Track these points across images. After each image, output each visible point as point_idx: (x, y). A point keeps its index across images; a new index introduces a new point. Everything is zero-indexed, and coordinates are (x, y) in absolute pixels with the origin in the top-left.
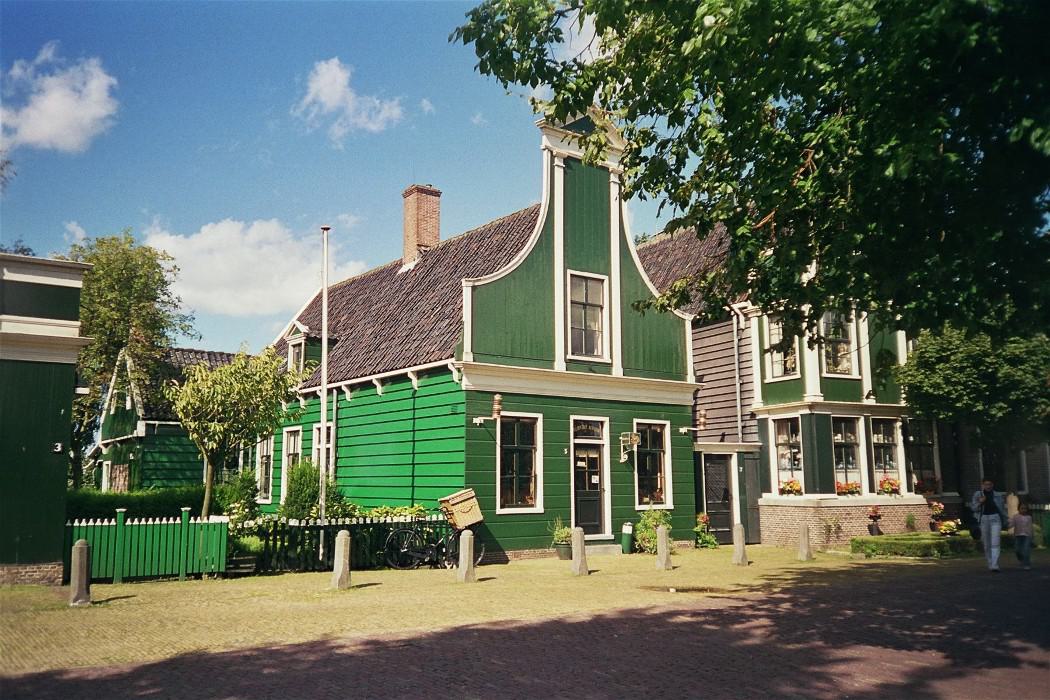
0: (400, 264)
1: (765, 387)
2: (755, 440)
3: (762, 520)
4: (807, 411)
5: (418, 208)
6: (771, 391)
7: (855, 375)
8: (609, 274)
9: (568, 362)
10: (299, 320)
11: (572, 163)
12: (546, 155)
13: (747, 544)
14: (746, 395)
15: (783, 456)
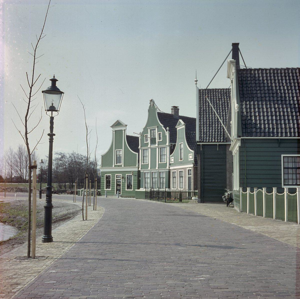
9: (115, 165)
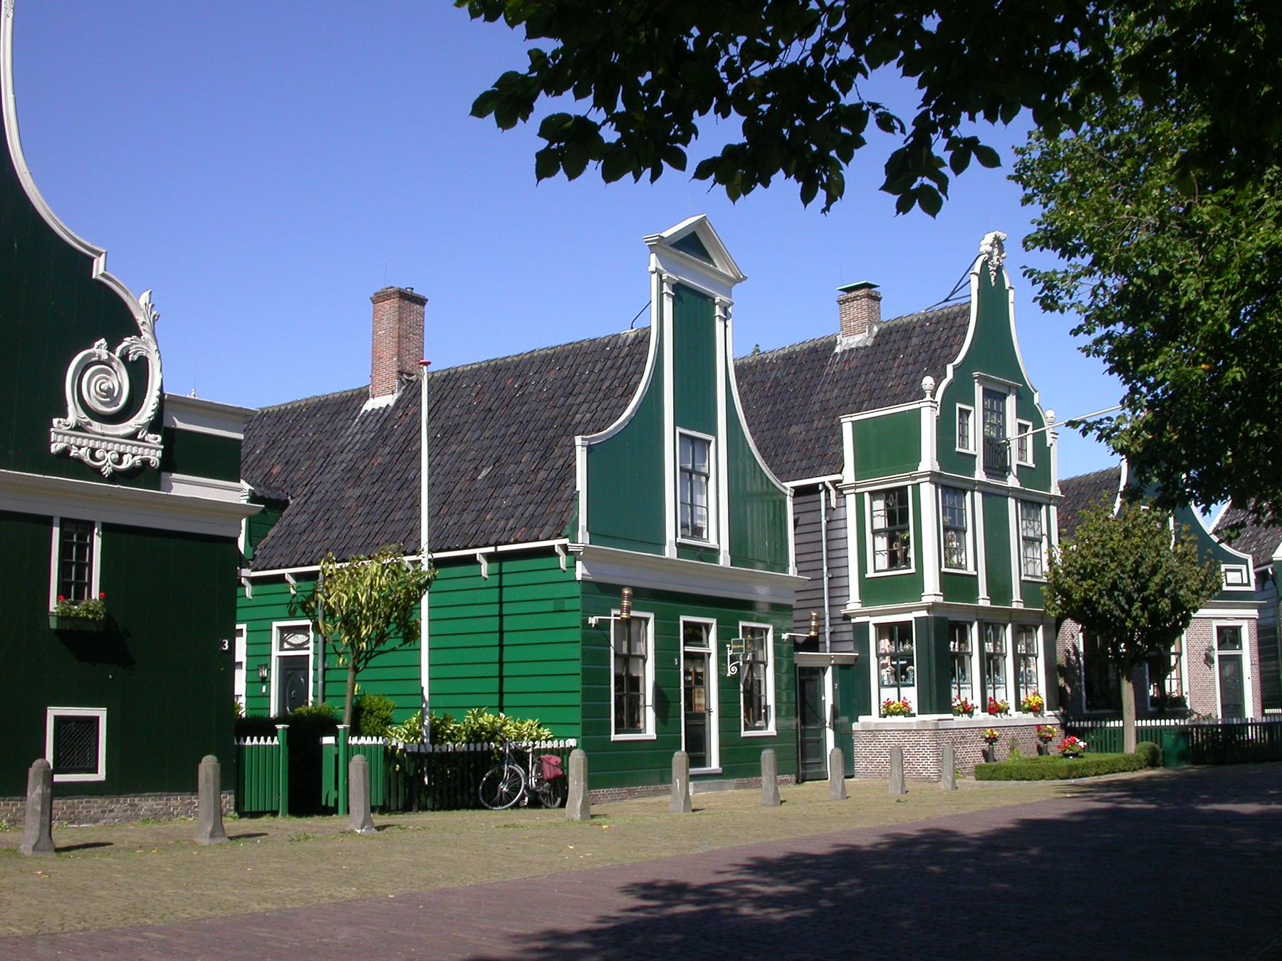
0: (363, 395)
1: (864, 583)
2: (849, 652)
3: (856, 750)
4: (924, 613)
5: (400, 320)
6: (873, 590)
7: (970, 570)
8: (714, 432)
9: (680, 546)
11: (685, 295)
12: (654, 277)
13: (846, 777)
14: (838, 593)
15: (884, 666)
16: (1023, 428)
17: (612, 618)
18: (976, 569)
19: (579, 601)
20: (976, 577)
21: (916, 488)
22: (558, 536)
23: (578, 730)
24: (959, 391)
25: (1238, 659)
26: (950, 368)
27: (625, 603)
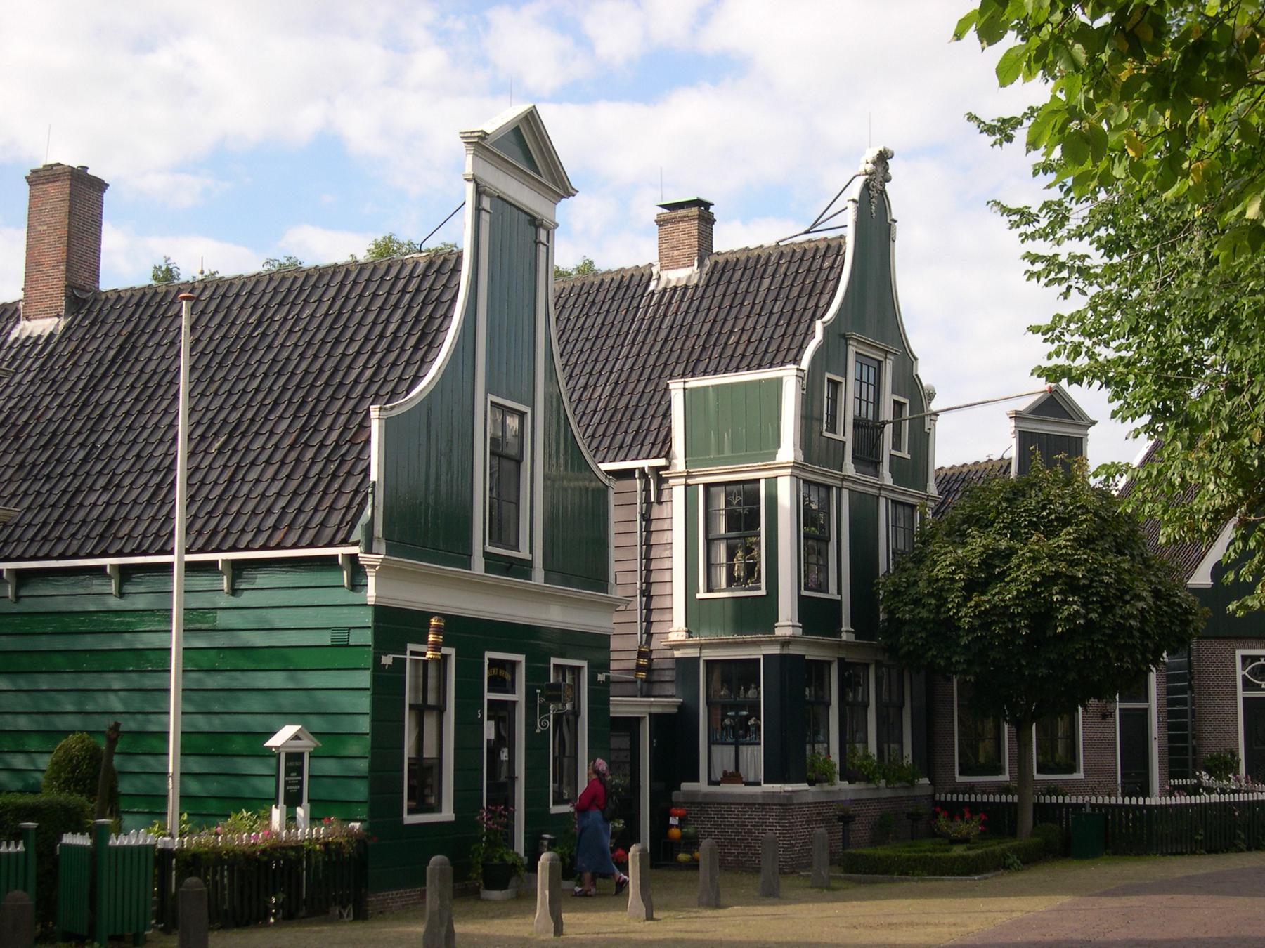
4: (776, 650)
9: (487, 555)
10: (650, 715)
16: (898, 406)
17: (408, 657)
18: (839, 592)
19: (369, 633)
20: (839, 603)
21: (772, 482)
22: (344, 542)
23: (363, 812)
24: (830, 356)
25: (1145, 713)
26: (819, 326)
27: (431, 638)
